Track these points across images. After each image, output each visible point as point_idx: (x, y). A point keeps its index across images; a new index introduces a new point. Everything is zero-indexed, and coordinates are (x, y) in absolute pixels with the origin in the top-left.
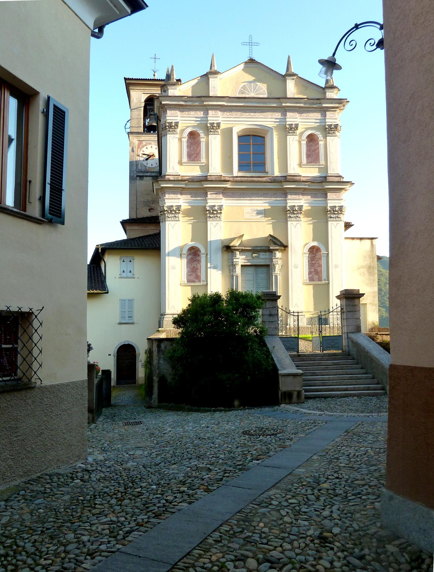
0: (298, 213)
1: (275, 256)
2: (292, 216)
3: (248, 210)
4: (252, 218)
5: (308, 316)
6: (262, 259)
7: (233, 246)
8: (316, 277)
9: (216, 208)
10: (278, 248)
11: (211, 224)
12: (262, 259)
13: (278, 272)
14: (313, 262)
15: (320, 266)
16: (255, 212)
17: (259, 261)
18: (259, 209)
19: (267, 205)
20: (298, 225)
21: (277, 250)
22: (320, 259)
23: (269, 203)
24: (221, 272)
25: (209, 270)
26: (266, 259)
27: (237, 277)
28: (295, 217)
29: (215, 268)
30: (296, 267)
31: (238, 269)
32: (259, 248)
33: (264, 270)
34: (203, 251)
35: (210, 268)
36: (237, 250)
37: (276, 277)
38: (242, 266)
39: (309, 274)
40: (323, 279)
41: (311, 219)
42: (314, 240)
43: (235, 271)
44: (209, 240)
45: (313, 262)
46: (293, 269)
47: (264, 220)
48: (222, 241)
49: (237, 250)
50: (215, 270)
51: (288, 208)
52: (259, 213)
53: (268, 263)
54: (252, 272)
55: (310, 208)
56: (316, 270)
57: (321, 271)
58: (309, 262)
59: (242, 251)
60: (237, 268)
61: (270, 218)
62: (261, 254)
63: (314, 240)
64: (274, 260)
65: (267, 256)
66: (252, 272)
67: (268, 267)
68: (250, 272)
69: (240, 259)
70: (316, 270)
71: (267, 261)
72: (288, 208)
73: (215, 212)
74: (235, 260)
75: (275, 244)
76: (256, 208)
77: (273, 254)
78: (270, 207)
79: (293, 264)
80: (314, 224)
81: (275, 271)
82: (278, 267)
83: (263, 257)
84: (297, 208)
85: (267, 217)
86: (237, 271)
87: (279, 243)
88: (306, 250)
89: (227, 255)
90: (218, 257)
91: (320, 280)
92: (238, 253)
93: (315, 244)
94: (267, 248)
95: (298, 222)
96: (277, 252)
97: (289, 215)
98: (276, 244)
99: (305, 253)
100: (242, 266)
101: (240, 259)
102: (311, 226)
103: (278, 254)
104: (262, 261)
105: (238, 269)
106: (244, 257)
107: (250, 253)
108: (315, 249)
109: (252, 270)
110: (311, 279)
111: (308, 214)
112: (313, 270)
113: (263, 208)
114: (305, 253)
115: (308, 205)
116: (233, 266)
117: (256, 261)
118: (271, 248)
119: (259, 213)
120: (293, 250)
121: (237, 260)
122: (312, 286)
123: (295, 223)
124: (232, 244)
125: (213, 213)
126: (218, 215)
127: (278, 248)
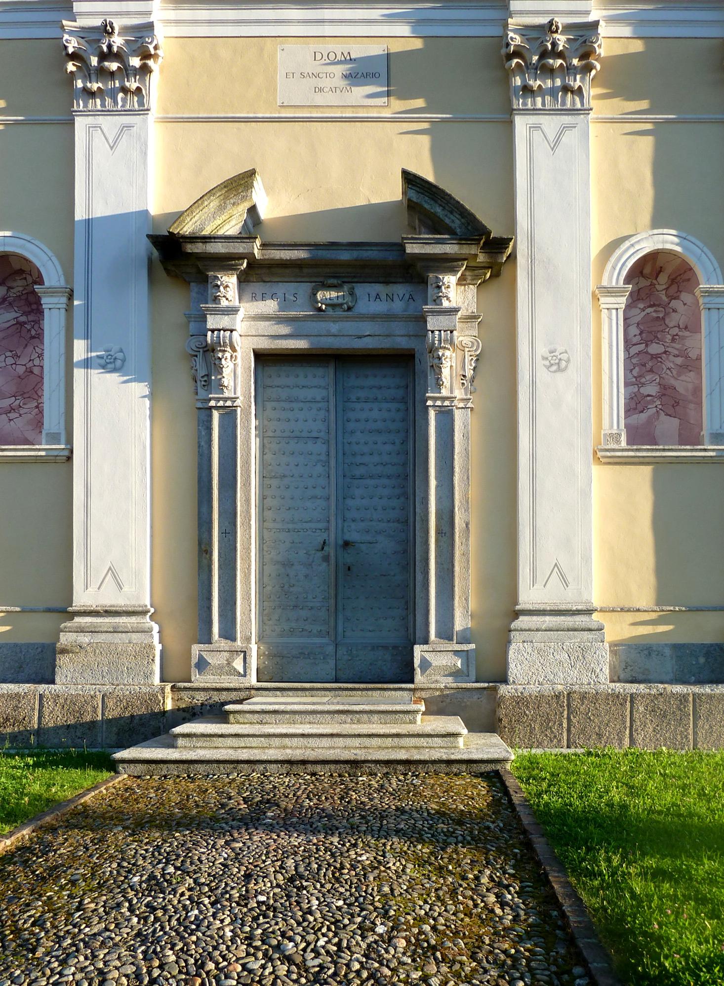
0: (569, 70)
1: (437, 300)
2: (535, 84)
3: (298, 57)
4: (319, 99)
5: (619, 629)
6: (368, 317)
7: (193, 239)
8: (668, 425)
9: (118, 41)
10: (450, 249)
11: (94, 135)
12: (368, 317)
13: (459, 393)
14: (655, 349)
15: (692, 365)
16: (339, 70)
17: (350, 327)
18: (359, 51)
19: (404, 30)
20: (569, 138)
21: (447, 263)
22: (693, 327)
23: (418, 23)
24: (141, 389)
25: (79, 374)
26: (388, 317)
27: (229, 415)
28: (553, 92)
29: (111, 363)
30: (557, 365)
31: (237, 375)
32: (345, 256)
33: (382, 382)
34: (52, 275)
35: (87, 364)
36: (225, 262)
37: (446, 416)
38: (262, 358)
39: (629, 411)
40: (705, 432)
41: (644, 104)
42: (658, 221)
43: (221, 387)
44: (80, 214)
45: (655, 349)
46: (542, 374)
47: (386, 114)
48: (155, 221)
49: (225, 262)
50: (115, 377)
51: (516, 40)
52: (360, 72)
53: (403, 343)
54: (319, 394)
55: (638, 46)
56: (666, 391)
57: (697, 390)
58: (628, 344)
59: (257, 274)
60: (228, 367)
61: (420, 103)
62: (362, 290)
63: (658, 221)
64: (432, 323)
65: (398, 306)
66: (319, 394)
67: (406, 365)
68: (309, 394)
69: (246, 321)
70: (666, 391)
71: (398, 328)
72: (516, 40)
73: (114, 66)
74: (212, 322)
75: (436, 227)
76: (339, 48)
77: (431, 291)
78: (418, 44)
79: (542, 349)
80: (658, 132)
81: (439, 385)
82: (451, 365)
83: (379, 307)
84: (562, 40)
85: (402, 97)
86: (227, 378)
87: (455, 222)
88: (616, 273)
89: (175, 302)
90: (132, 306)
91: (690, 437)
92: (229, 281)
93: (668, 240)
94: (391, 257)
95: (567, 119)
96: (450, 279)
97: (518, 81)
98: (452, 229)
99: (609, 291)
100: (262, 358)
101: (246, 321)
102: (646, 145)
103: (455, 292)
104: (367, 328)
105: (237, 375)
106: (270, 306)
107: (304, 289)
108: (663, 279)
109: (316, 383)
110: (638, 435)
111: (624, 79)
112: (652, 389)
113: (376, 49)
114: (609, 291)
115: (627, 31)
116: (206, 355)
117: (334, 328)
118: (412, 249)
119: (360, 72)
120: (539, 272)
121: (223, 321)
122: (647, 470)
123: (550, 124)
124: (187, 228)
125: (102, 73)
126: (133, 85)
127: (450, 249)
